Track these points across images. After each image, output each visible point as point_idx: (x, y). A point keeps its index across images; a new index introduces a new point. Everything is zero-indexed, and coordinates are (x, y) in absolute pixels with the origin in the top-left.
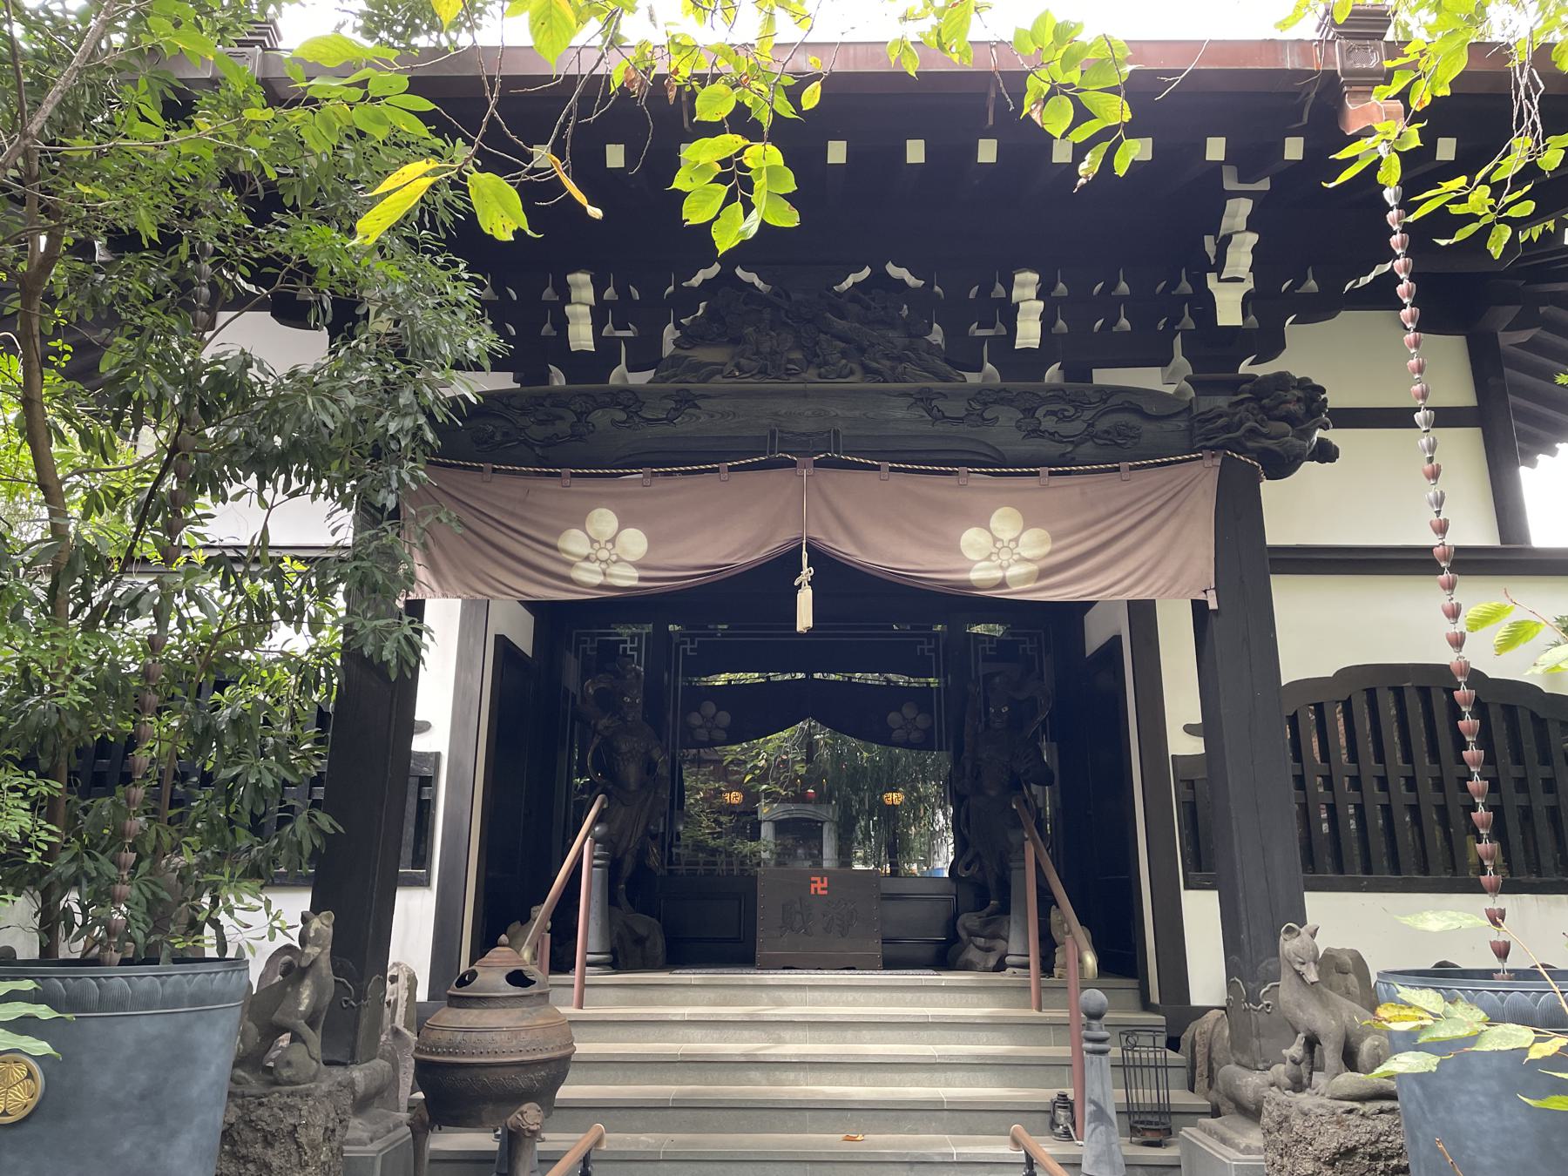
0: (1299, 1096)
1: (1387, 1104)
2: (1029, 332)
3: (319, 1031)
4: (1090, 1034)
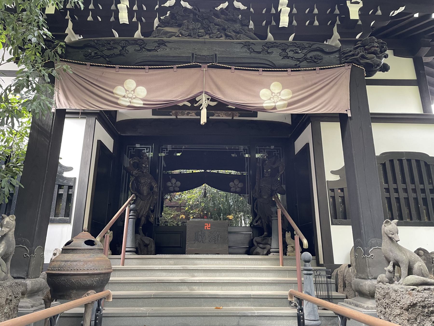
0: (392, 285)
1: (427, 287)
2: (284, 21)
3: (9, 263)
4: (306, 268)
